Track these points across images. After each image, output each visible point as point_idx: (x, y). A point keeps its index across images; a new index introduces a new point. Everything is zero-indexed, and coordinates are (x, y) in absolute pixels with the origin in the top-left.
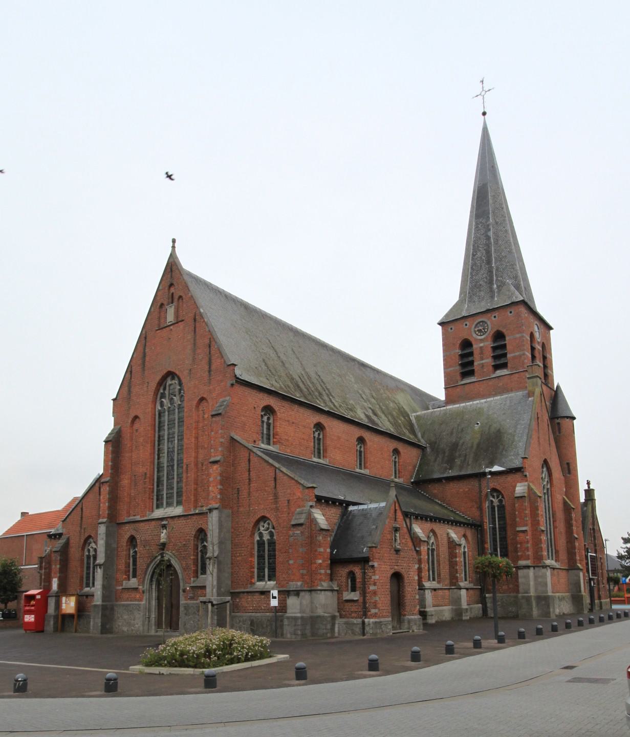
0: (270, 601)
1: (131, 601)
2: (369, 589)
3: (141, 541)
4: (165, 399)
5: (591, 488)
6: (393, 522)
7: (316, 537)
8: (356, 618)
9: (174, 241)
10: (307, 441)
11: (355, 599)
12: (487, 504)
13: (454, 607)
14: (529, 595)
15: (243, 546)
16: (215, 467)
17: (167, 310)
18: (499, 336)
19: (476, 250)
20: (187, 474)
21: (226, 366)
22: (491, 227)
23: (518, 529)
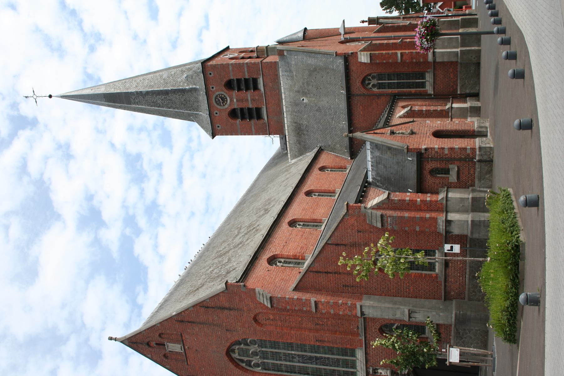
0: (455, 253)
2: (447, 155)
4: (253, 361)
5: (367, 19)
6: (385, 135)
7: (395, 203)
8: (475, 170)
10: (304, 233)
11: (456, 169)
12: (375, 90)
13: (469, 114)
14: (459, 52)
17: (170, 351)
18: (229, 85)
19: (155, 104)
20: (325, 341)
21: (226, 291)
23: (399, 60)
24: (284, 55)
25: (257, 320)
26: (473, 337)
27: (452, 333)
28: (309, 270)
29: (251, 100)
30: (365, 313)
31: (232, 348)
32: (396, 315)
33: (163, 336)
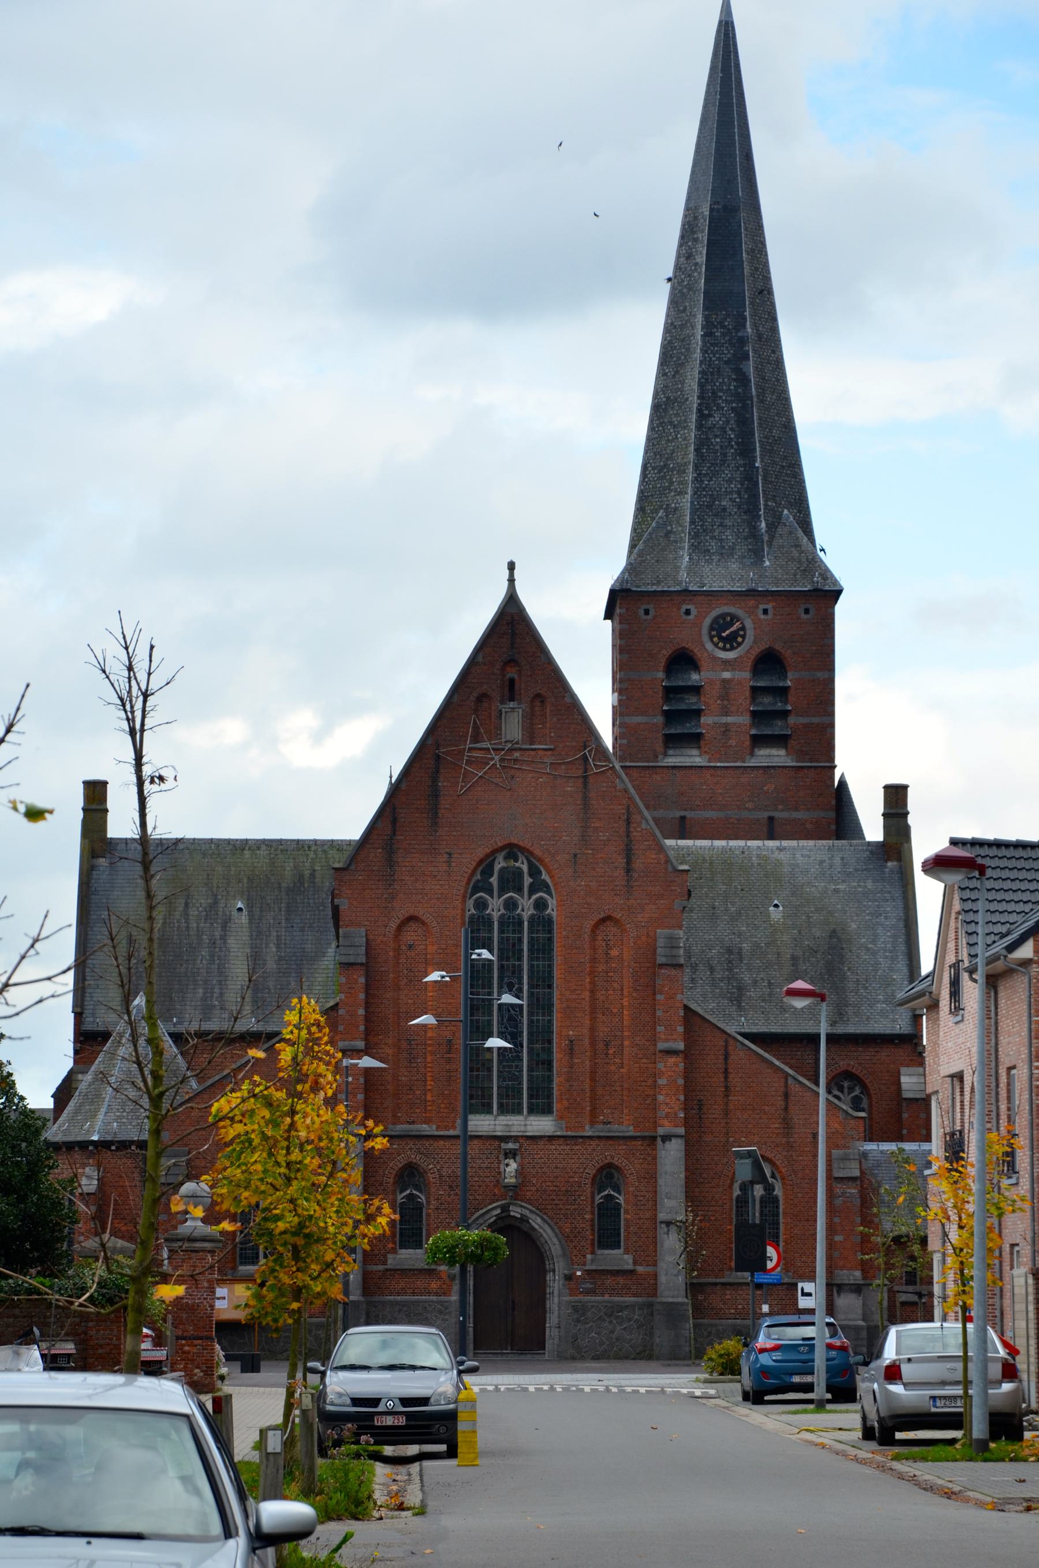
1: (414, 1294)
3: (441, 1176)
9: (511, 566)
15: (714, 1203)
16: (672, 1060)
20: (572, 1058)
22: (750, 348)
24: (886, 861)
25: (604, 922)
26: (614, 1336)
27: (617, 1298)
28: (729, 1039)
29: (726, 725)
30: (667, 1142)
31: (520, 854)
32: (669, 1198)
33: (537, 703)
